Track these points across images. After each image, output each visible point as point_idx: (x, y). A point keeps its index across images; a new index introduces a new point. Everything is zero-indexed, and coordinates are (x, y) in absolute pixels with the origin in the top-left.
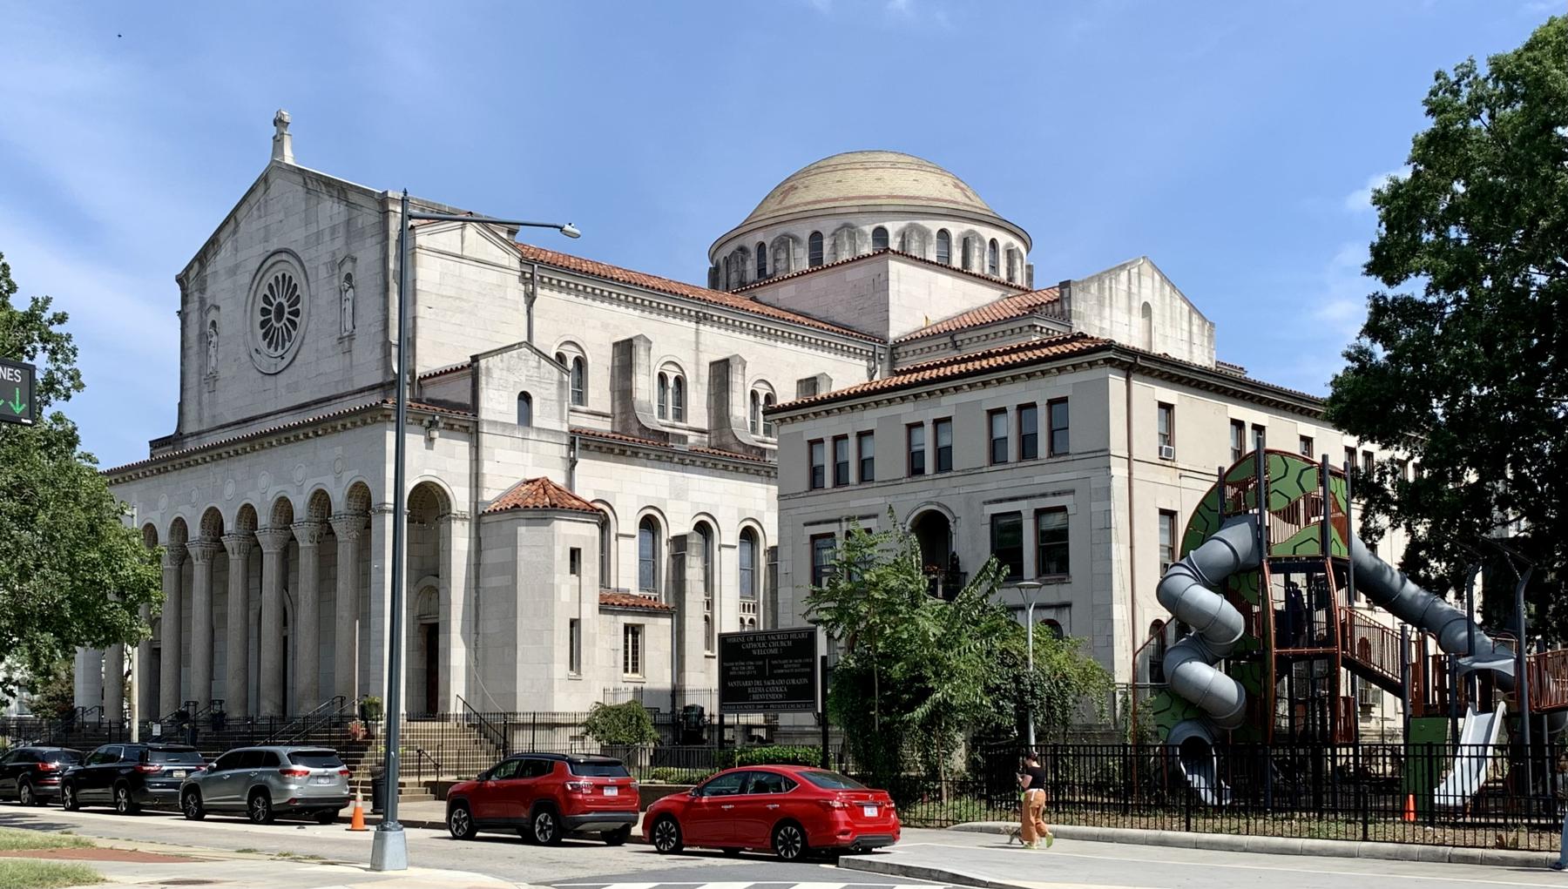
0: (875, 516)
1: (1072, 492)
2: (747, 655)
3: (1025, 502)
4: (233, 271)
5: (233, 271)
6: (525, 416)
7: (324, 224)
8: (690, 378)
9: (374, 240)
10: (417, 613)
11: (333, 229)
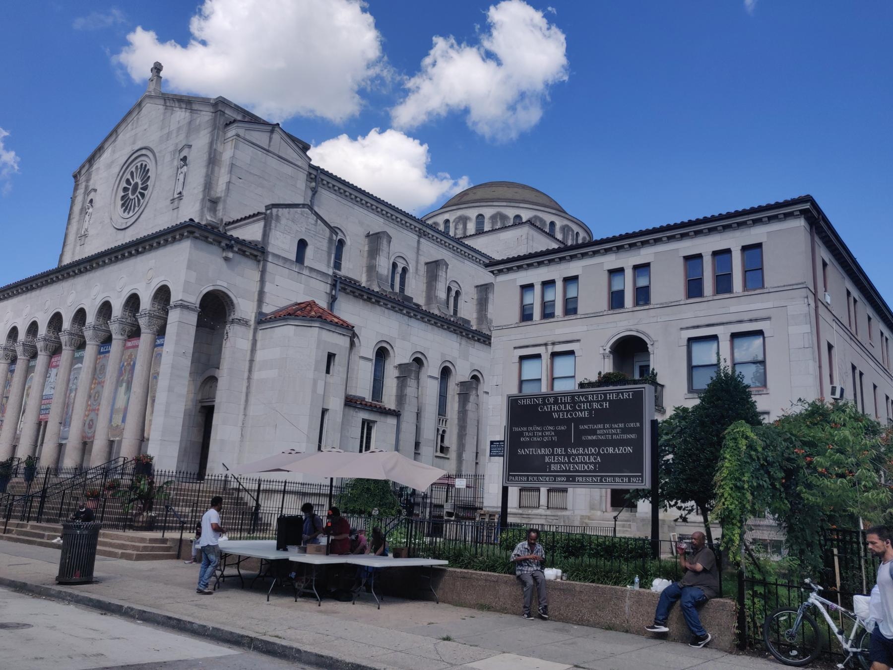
0: (578, 341)
1: (769, 318)
2: (546, 419)
3: (721, 327)
4: (109, 166)
5: (109, 166)
6: (300, 258)
7: (174, 126)
8: (411, 269)
9: (206, 131)
10: (199, 398)
11: (179, 129)
